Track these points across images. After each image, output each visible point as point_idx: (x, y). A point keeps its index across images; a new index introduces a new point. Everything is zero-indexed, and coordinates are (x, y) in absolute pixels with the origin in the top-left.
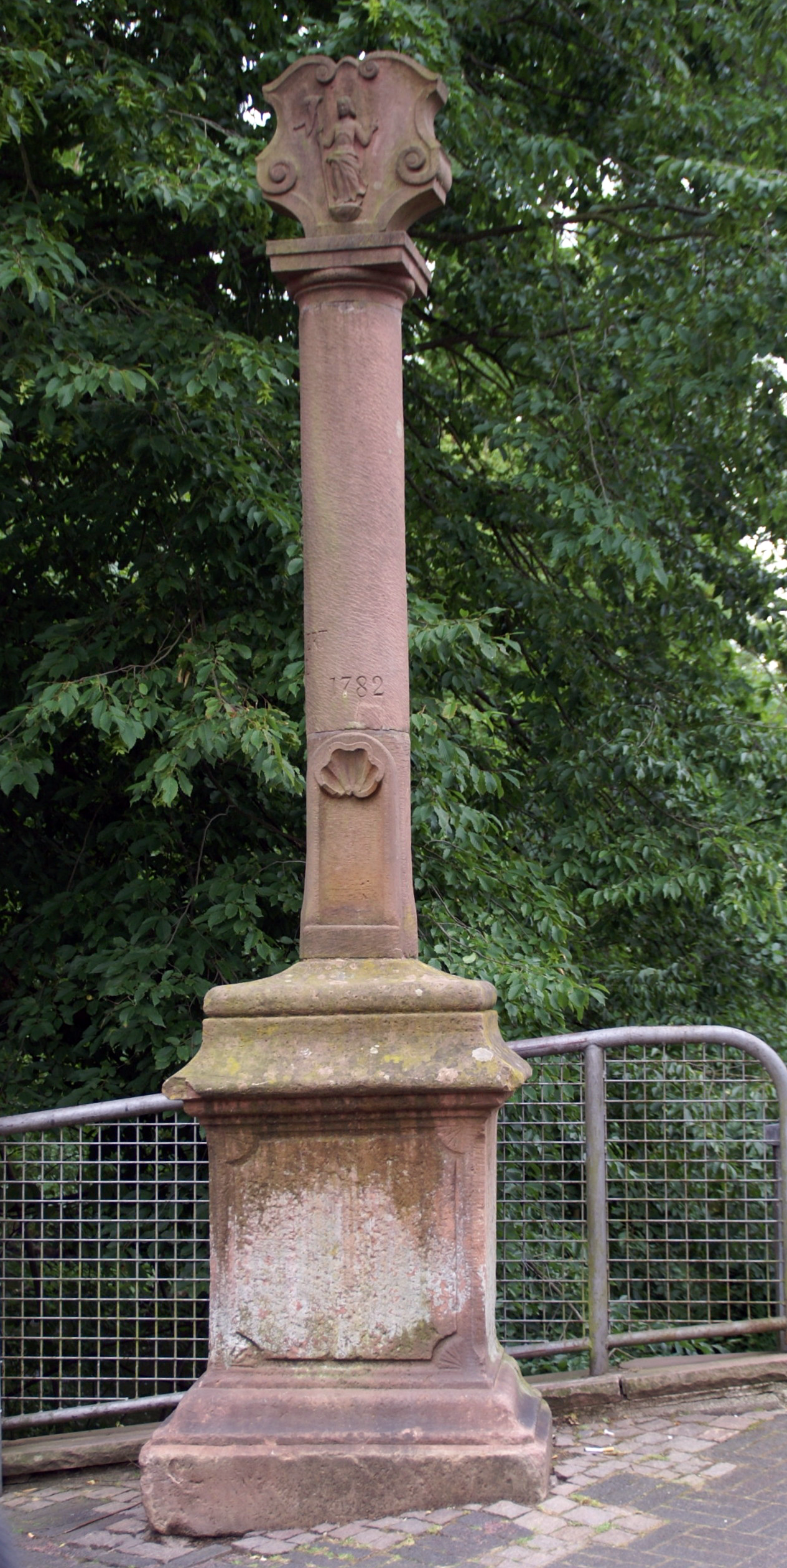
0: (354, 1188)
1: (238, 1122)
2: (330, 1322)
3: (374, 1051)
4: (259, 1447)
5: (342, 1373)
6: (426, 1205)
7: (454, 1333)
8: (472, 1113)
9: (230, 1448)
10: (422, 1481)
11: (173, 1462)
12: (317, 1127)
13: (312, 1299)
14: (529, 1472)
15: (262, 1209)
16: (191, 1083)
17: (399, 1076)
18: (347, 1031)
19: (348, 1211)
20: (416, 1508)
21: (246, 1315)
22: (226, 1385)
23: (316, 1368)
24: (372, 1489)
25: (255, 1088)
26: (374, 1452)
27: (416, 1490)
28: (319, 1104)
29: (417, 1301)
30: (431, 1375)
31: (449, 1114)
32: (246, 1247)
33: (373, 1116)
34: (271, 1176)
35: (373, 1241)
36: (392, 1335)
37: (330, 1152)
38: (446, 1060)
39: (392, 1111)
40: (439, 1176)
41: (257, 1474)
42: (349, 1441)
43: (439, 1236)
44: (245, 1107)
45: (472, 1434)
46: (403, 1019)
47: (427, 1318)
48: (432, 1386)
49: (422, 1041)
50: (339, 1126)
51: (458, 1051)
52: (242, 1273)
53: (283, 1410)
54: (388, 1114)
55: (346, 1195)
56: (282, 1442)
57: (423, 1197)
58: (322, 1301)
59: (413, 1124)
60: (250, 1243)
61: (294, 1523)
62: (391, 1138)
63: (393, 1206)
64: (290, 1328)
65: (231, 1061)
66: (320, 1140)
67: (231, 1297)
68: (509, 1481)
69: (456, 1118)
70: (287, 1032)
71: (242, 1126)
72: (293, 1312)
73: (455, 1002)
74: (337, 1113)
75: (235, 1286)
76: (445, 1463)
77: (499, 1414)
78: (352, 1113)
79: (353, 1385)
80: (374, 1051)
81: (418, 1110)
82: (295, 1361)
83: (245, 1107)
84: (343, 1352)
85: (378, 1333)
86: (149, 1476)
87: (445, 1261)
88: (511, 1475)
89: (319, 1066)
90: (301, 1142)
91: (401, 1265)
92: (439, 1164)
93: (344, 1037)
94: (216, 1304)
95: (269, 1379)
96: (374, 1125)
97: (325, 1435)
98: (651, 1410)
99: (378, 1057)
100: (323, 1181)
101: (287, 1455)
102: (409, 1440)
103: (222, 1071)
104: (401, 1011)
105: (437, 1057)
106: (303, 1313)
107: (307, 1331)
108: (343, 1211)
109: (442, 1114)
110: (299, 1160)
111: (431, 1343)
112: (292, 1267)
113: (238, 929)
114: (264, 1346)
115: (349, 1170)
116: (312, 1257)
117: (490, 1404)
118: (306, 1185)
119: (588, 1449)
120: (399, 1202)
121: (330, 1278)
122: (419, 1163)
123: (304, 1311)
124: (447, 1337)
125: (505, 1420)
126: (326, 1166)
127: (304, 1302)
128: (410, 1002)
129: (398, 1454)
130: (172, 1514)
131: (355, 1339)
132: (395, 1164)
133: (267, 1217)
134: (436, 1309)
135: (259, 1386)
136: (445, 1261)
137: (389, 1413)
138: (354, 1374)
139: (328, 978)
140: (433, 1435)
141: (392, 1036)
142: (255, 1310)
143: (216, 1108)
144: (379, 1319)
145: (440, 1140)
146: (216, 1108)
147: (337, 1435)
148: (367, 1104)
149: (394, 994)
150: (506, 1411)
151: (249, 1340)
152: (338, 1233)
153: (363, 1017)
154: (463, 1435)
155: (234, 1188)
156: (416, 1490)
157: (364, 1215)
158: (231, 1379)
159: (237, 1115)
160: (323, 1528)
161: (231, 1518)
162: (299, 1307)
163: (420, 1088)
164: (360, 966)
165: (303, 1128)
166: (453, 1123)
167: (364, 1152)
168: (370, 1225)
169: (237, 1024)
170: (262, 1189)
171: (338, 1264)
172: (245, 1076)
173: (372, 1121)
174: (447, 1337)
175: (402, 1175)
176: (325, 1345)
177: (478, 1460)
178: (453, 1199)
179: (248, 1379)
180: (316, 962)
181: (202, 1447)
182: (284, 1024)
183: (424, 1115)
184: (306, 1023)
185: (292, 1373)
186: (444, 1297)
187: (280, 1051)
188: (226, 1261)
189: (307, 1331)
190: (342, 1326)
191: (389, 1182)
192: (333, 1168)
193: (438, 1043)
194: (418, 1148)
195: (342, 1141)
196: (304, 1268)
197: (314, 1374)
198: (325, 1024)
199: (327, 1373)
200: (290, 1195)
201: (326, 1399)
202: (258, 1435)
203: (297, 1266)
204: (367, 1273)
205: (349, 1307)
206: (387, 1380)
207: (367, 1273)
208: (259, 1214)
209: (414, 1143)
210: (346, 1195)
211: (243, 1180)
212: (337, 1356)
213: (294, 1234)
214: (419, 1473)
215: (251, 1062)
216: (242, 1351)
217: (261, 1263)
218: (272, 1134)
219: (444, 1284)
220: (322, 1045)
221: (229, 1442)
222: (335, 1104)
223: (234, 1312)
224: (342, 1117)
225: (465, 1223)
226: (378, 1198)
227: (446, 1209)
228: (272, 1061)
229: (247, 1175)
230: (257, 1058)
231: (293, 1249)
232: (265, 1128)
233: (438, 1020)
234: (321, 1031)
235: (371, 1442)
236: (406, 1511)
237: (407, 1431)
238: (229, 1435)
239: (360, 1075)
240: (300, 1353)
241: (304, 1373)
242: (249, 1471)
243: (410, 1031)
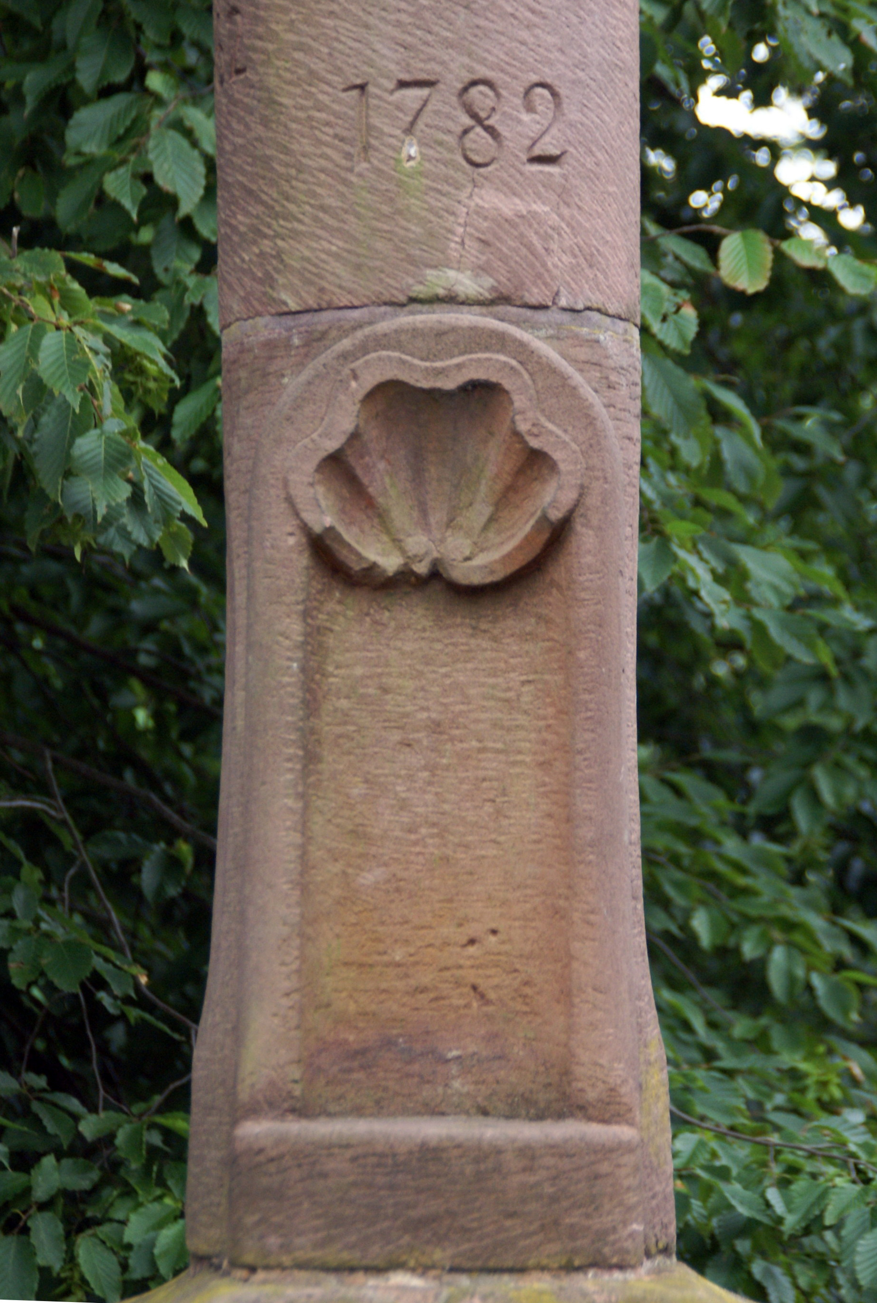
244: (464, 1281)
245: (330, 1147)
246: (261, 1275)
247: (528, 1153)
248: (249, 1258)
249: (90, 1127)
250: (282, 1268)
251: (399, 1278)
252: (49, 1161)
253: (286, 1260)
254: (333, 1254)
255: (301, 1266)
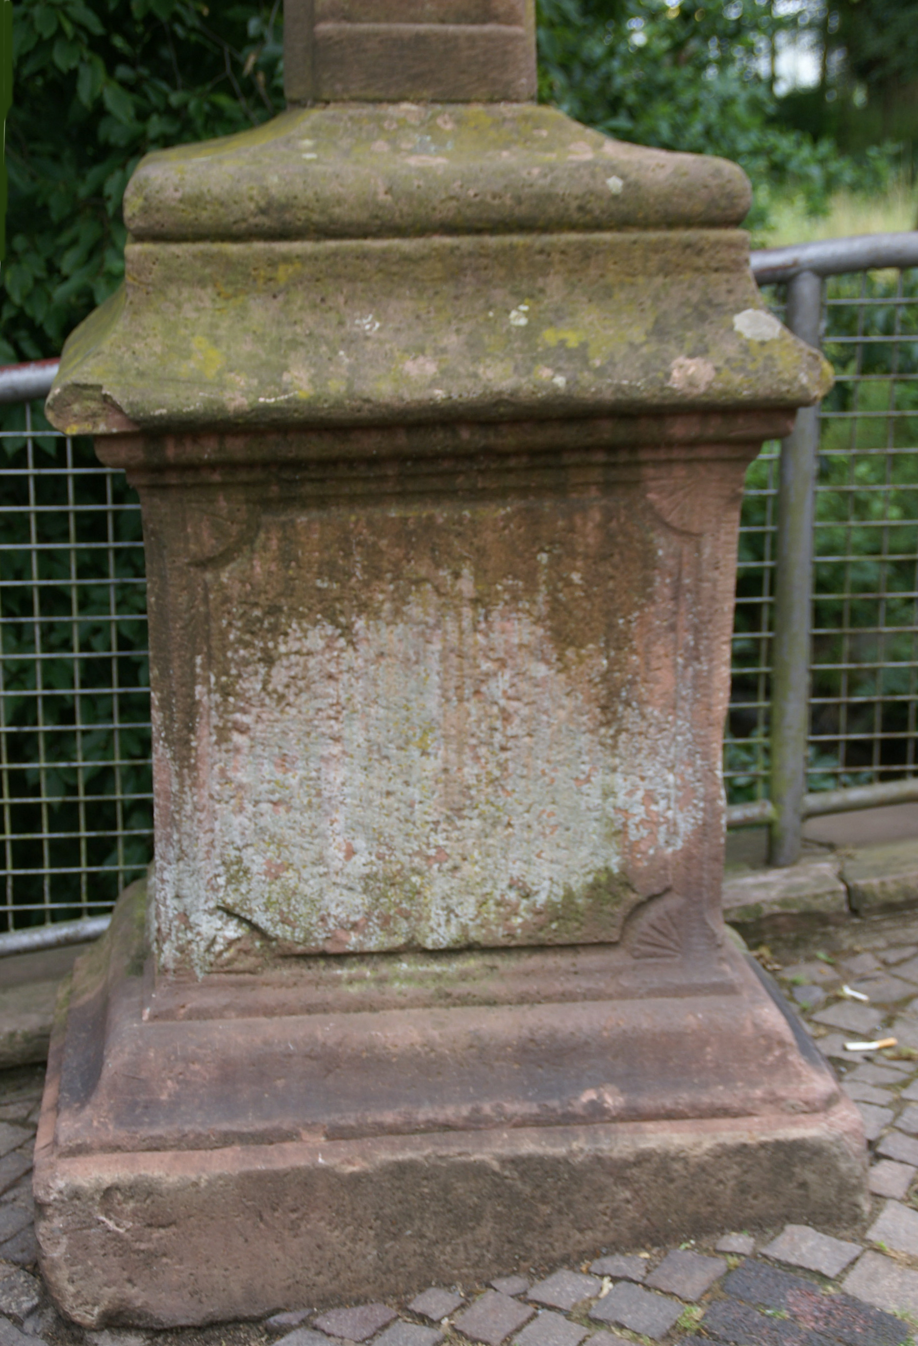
0: (467, 611)
1: (216, 477)
2: (415, 879)
3: (518, 319)
4: (288, 1146)
5: (439, 977)
6: (617, 641)
7: (668, 890)
8: (725, 452)
9: (228, 1152)
10: (628, 1194)
11: (108, 1192)
12: (389, 487)
13: (377, 837)
14: (843, 1166)
15: (269, 660)
16: (117, 398)
17: (586, 377)
18: (455, 274)
19: (454, 660)
20: (615, 1247)
21: (237, 872)
22: (201, 1014)
23: (385, 969)
24: (530, 1221)
25: (266, 408)
26: (530, 1145)
27: (615, 1213)
28: (402, 440)
29: (593, 830)
30: (618, 972)
31: (676, 454)
32: (236, 737)
33: (512, 462)
34: (289, 590)
35: (506, 717)
36: (541, 898)
37: (413, 539)
38: (681, 341)
39: (555, 451)
40: (648, 582)
41: (289, 1201)
42: (476, 1124)
43: (643, 703)
44: (237, 448)
45: (720, 1095)
46: (581, 246)
47: (615, 864)
48: (625, 995)
49: (620, 296)
50: (437, 483)
51: (702, 318)
52: (228, 791)
53: (328, 1062)
54: (546, 458)
55: (450, 625)
56: (336, 1134)
57: (611, 626)
58: (399, 840)
59: (596, 475)
60: (243, 730)
61: (367, 1289)
62: (547, 505)
63: (548, 647)
64: (332, 895)
65: (199, 343)
66: (394, 513)
67: (204, 839)
68: (803, 1185)
69: (688, 462)
70: (324, 277)
71: (223, 485)
72: (337, 864)
73: (695, 206)
74: (438, 457)
75: (214, 815)
76: (674, 1159)
77: (769, 1049)
78: (470, 456)
79: (465, 1001)
80: (518, 319)
81: (611, 448)
82: (341, 957)
83: (237, 448)
84: (442, 934)
85: (512, 896)
86: (58, 1222)
87: (654, 751)
88: (809, 1176)
89: (403, 356)
90: (354, 518)
91: (561, 763)
92: (648, 560)
93: (448, 289)
94: (172, 854)
95: (290, 996)
96: (511, 480)
97: (425, 1113)
98: (901, 934)
99: (529, 333)
100: (400, 599)
101: (349, 1160)
102: (596, 1114)
103: (186, 368)
104: (573, 227)
105: (659, 331)
106: (359, 864)
107: (367, 900)
108: (443, 659)
109: (662, 455)
110: (348, 555)
111: (620, 911)
112: (336, 775)
113: (63, 59)
114: (279, 931)
115: (457, 575)
116: (376, 753)
117: (749, 1031)
118: (364, 608)
119: (853, 1046)
120: (563, 635)
121: (415, 793)
122: (605, 557)
123: (359, 859)
124: (653, 898)
125: (783, 1061)
126: (408, 568)
127: (360, 843)
128: (596, 207)
129: (578, 1145)
130: (109, 1291)
131: (468, 910)
132: (556, 561)
133: (280, 676)
134: (633, 847)
135: (269, 1012)
136: (654, 751)
137: (548, 1060)
138: (464, 976)
139: (396, 150)
140: (646, 1102)
141: (555, 284)
142: (256, 862)
143: (171, 451)
144: (516, 870)
145: (650, 507)
146: (171, 451)
147: (449, 1113)
148: (509, 439)
149: (561, 188)
150: (782, 1043)
151: (242, 920)
152: (432, 703)
153: (493, 241)
154: (705, 1099)
155: (207, 618)
156: (615, 1213)
157: (486, 666)
158: (211, 1000)
159: (213, 466)
160: (435, 1302)
161: (237, 1291)
162: (351, 853)
163: (632, 403)
164: (459, 122)
165: (359, 488)
166: (680, 472)
167: (489, 536)
168: (499, 686)
169: (208, 259)
170: (269, 619)
171: (432, 765)
172: (241, 380)
173: (509, 471)
174: (653, 898)
175: (569, 583)
176: (404, 925)
177: (743, 1149)
178: (673, 628)
179: (248, 997)
180: (354, 110)
181: (168, 1155)
182: (314, 257)
183: (623, 457)
184: (364, 256)
185: (337, 980)
186: (651, 822)
187: (310, 319)
188: (193, 768)
189: (367, 900)
190: (440, 886)
191: (540, 598)
192: (423, 572)
193: (656, 299)
194: (602, 526)
195: (441, 514)
196: (360, 777)
197: (381, 980)
198: (406, 258)
199: (409, 978)
200: (330, 630)
201: (415, 1036)
202: (286, 1123)
203: (344, 772)
204: (493, 781)
205: (453, 849)
206: (532, 986)
207: (493, 781)
208: (262, 670)
209: (597, 516)
210: (450, 625)
211: (227, 600)
212: (429, 944)
213: (339, 710)
214: (625, 1182)
215: (246, 347)
216: (230, 943)
217: (267, 769)
218: (288, 501)
219: (650, 798)
220: (403, 306)
221: (227, 1140)
222: (439, 440)
223: (210, 867)
224: (446, 465)
225: (697, 675)
226: (518, 630)
227: (659, 649)
228: (294, 344)
229: (235, 590)
230: (259, 338)
231: (337, 739)
232: (274, 490)
233: (656, 248)
234: (396, 275)
235: (522, 1123)
236: (595, 1254)
237: (590, 1095)
238: (225, 1126)
239: (498, 376)
240: (353, 941)
241: (361, 979)
242: (271, 1198)
243: (593, 272)
244: (438, 107)
245: (368, 36)
246: (332, 105)
247: (472, 39)
248: (326, 96)
249: (175, 99)
250: (343, 101)
251: (405, 106)
252: (154, 118)
253: (346, 96)
254: (371, 93)
255: (354, 99)
